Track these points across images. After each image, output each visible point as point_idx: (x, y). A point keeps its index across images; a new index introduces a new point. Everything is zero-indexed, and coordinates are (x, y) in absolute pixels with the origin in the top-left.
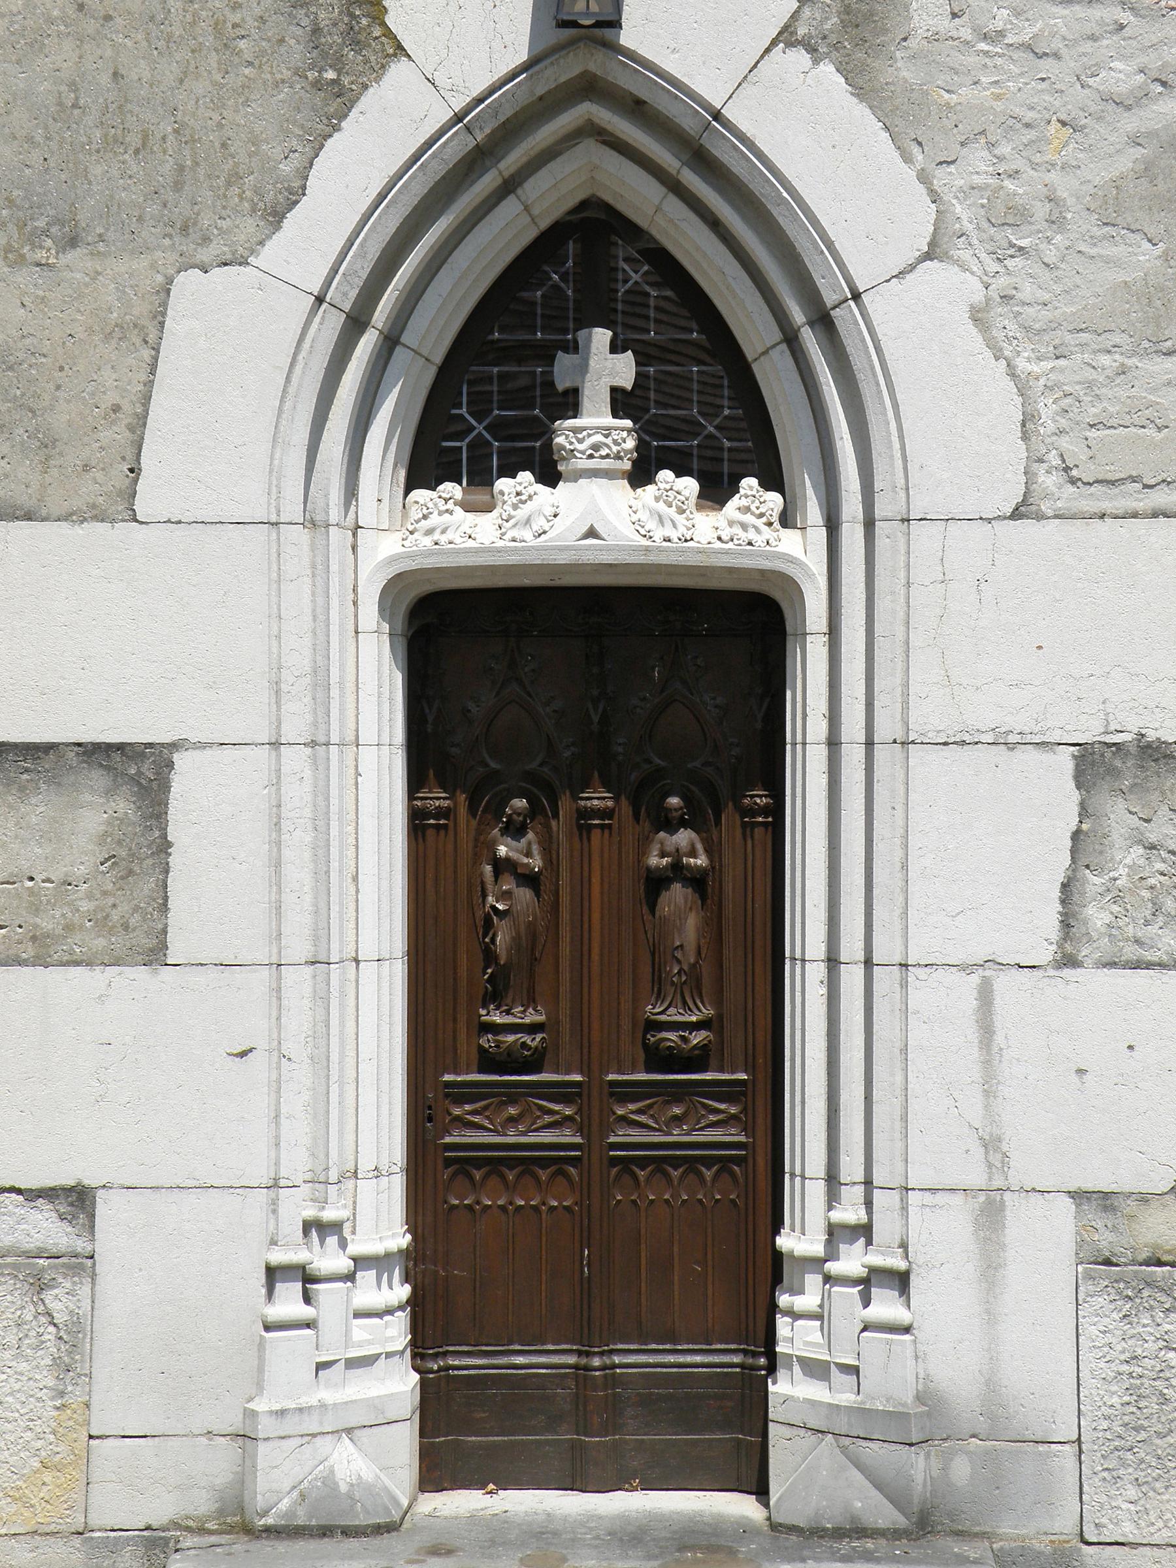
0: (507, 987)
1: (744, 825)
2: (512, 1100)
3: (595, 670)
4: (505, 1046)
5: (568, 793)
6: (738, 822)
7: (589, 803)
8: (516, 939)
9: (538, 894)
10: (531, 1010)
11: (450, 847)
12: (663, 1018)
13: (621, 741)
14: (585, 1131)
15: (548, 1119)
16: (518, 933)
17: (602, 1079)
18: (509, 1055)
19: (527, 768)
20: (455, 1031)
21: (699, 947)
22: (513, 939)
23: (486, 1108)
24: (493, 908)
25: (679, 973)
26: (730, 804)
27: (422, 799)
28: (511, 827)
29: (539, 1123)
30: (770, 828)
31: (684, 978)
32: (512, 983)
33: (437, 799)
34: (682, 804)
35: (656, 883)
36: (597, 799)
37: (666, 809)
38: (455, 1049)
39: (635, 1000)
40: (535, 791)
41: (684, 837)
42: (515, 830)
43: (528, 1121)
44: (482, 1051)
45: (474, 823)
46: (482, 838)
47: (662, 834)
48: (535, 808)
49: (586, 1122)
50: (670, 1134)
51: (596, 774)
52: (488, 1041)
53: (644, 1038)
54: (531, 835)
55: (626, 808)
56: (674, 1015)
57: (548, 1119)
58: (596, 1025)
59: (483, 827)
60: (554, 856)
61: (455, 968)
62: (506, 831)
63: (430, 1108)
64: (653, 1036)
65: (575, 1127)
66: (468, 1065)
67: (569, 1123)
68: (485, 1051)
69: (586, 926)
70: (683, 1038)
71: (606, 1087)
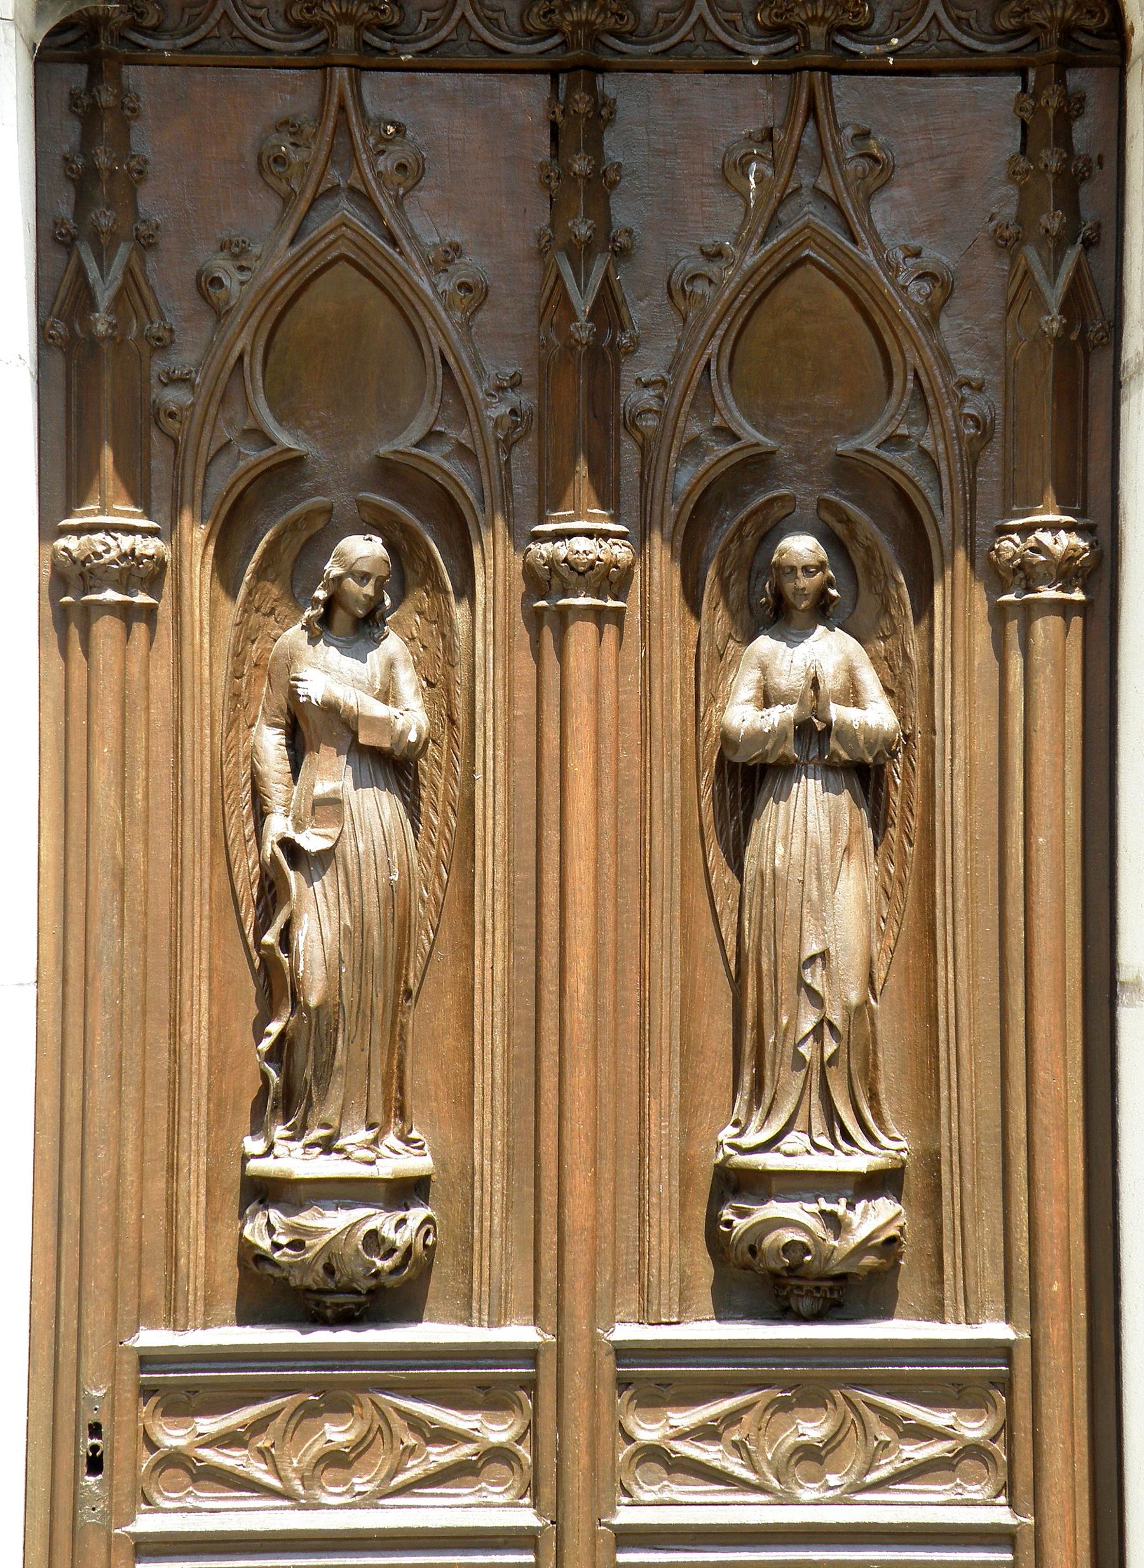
0: (324, 1072)
1: (999, 615)
2: (336, 1402)
3: (580, 165)
4: (316, 1244)
5: (500, 523)
6: (981, 607)
7: (562, 549)
8: (355, 935)
9: (413, 812)
10: (391, 1140)
11: (162, 675)
12: (771, 1161)
13: (648, 374)
14: (548, 1492)
15: (441, 1456)
16: (360, 917)
17: (595, 1341)
18: (329, 1270)
19: (384, 450)
20: (171, 1201)
21: (871, 963)
22: (345, 934)
23: (259, 1426)
24: (289, 846)
25: (817, 1032)
26: (961, 556)
27: (79, 531)
28: (340, 616)
29: (414, 1470)
30: (1077, 622)
31: (830, 1048)
32: (340, 1059)
33: (117, 527)
34: (823, 555)
35: (745, 781)
36: (586, 537)
37: (779, 567)
38: (172, 1256)
39: (687, 1111)
40: (408, 516)
41: (828, 651)
42: (352, 624)
43: (381, 1461)
44: (251, 1259)
45: (230, 611)
46: (254, 651)
47: (764, 644)
48: (405, 568)
49: (548, 1465)
50: (790, 1500)
51: (582, 468)
52: (261, 1230)
53: (713, 1219)
54: (393, 644)
55: (663, 568)
56: (799, 1154)
57: (441, 1456)
58: (579, 1182)
59: (255, 619)
60: (460, 703)
61: (175, 1021)
62: (323, 626)
63: (95, 1430)
64: (743, 1214)
65: (516, 1482)
66: (209, 1302)
67: (499, 1469)
68: (262, 1258)
69: (551, 898)
70: (834, 1222)
71: (608, 1364)
